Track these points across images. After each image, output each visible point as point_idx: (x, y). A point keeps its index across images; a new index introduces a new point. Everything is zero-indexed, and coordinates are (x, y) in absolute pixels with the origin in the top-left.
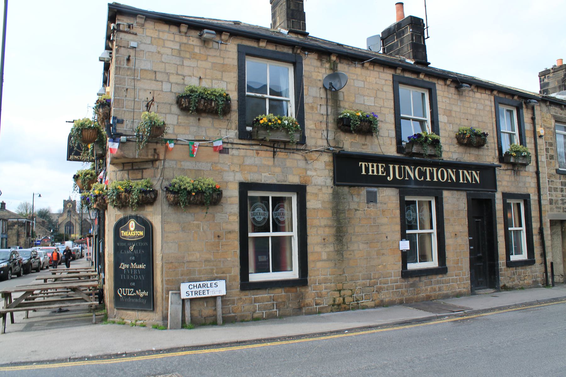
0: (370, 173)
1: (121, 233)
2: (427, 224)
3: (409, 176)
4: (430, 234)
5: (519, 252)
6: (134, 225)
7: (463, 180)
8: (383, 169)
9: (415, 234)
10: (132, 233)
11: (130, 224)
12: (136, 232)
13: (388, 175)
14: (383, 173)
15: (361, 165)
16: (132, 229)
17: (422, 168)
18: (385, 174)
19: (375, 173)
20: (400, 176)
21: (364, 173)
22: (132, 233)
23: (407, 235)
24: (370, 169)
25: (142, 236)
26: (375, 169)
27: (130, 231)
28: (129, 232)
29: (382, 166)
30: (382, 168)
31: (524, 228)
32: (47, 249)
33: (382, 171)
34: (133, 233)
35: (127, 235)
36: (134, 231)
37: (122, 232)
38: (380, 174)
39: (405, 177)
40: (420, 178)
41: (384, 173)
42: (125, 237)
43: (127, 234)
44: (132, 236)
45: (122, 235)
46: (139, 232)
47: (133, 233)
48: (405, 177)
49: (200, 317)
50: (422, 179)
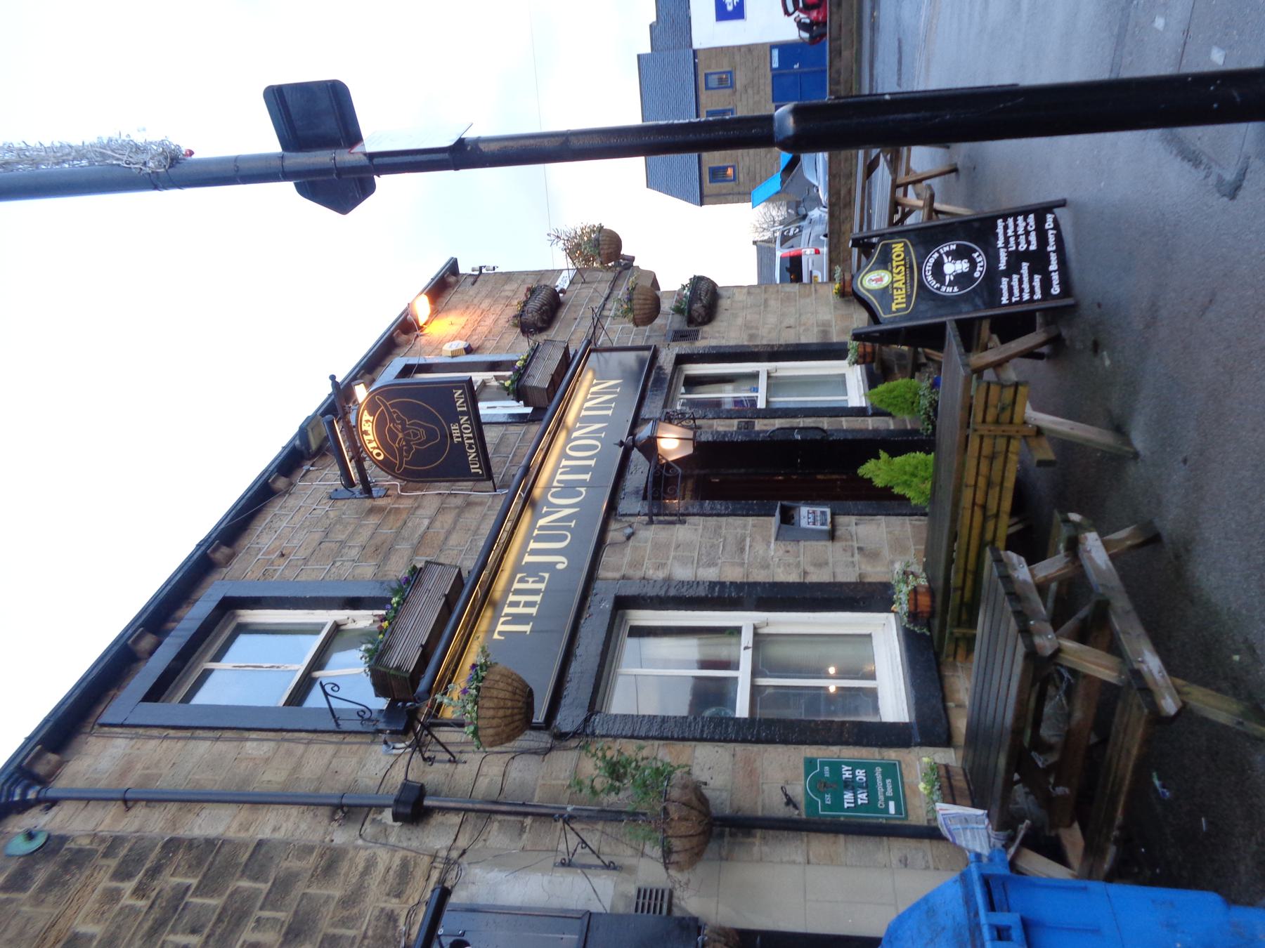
0: (533, 611)
1: (898, 310)
2: (720, 649)
3: (568, 518)
4: (760, 639)
5: (840, 383)
6: (874, 275)
7: (609, 408)
8: (531, 580)
9: (755, 690)
10: (898, 277)
11: (874, 286)
12: (895, 264)
13: (550, 567)
14: (541, 580)
15: (500, 633)
16: (886, 278)
17: (554, 490)
18: (547, 575)
19: (538, 598)
20: (563, 538)
21: (527, 628)
22: (898, 277)
23: (760, 714)
24: (520, 610)
25: (906, 246)
26: (523, 599)
27: (892, 283)
28: (895, 285)
29: (522, 580)
30: (527, 582)
31: (762, 367)
32: (960, 313)
33: (533, 582)
34: (899, 273)
35: (904, 291)
36: (891, 272)
37: (894, 307)
38: (542, 586)
39: (567, 528)
40: (580, 494)
41: (544, 578)
42: (909, 297)
43: (899, 292)
44: (906, 275)
45: (904, 305)
46: (894, 256)
47: (899, 273)
48: (567, 528)
49: (1227, 617)
50: (583, 490)
